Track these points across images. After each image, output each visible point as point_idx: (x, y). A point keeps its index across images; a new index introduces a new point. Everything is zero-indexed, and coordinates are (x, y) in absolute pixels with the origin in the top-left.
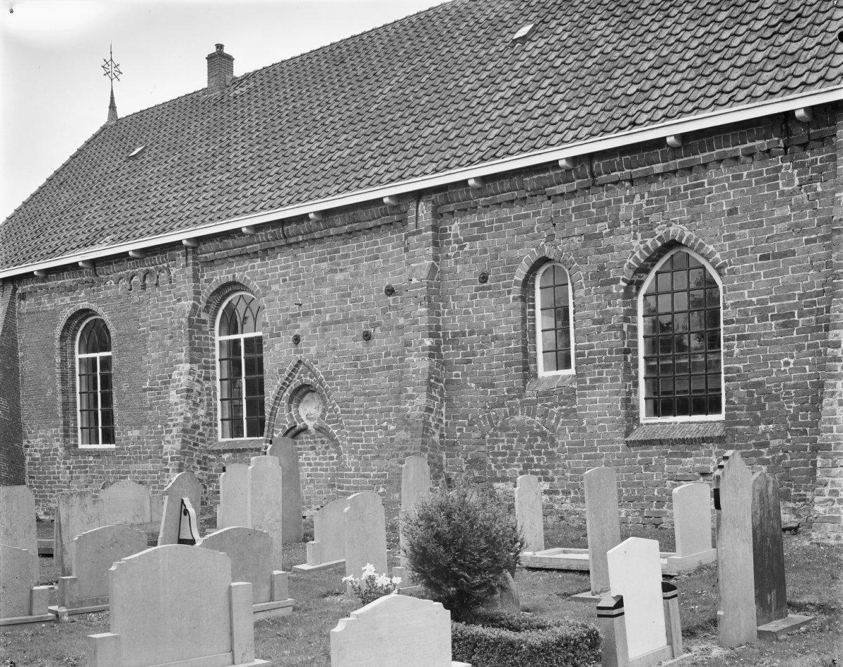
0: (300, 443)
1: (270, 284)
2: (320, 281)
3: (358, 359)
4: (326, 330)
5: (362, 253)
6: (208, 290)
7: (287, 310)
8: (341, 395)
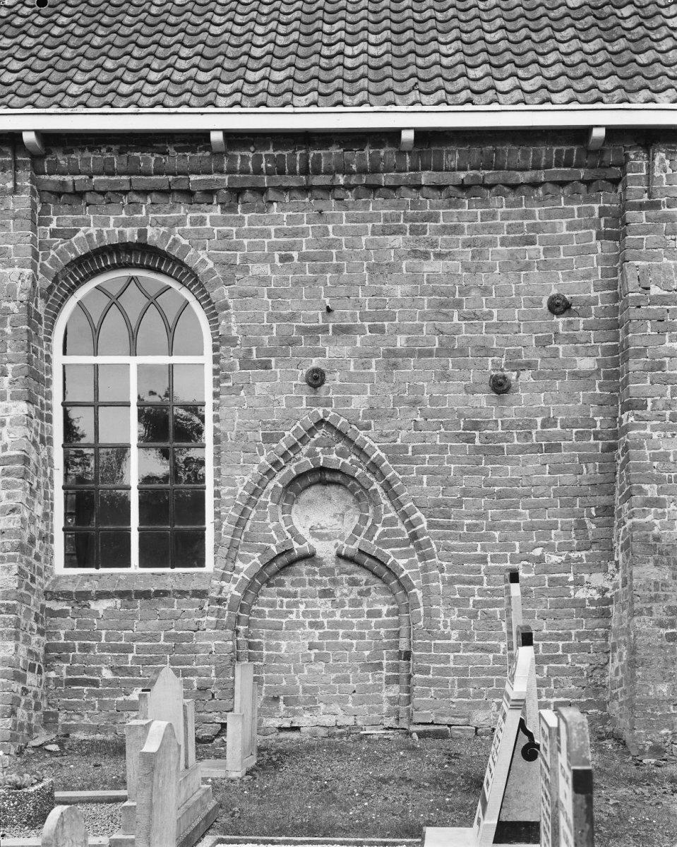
0: (293, 584)
1: (245, 259)
2: (381, 270)
3: (476, 426)
4: (395, 366)
5: (496, 229)
6: (61, 253)
7: (293, 317)
8: (428, 490)
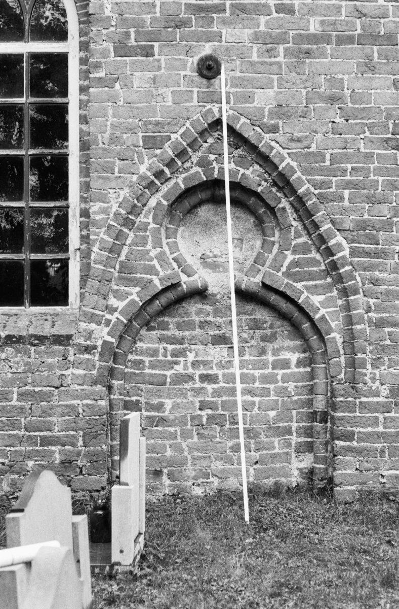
0: (179, 327)
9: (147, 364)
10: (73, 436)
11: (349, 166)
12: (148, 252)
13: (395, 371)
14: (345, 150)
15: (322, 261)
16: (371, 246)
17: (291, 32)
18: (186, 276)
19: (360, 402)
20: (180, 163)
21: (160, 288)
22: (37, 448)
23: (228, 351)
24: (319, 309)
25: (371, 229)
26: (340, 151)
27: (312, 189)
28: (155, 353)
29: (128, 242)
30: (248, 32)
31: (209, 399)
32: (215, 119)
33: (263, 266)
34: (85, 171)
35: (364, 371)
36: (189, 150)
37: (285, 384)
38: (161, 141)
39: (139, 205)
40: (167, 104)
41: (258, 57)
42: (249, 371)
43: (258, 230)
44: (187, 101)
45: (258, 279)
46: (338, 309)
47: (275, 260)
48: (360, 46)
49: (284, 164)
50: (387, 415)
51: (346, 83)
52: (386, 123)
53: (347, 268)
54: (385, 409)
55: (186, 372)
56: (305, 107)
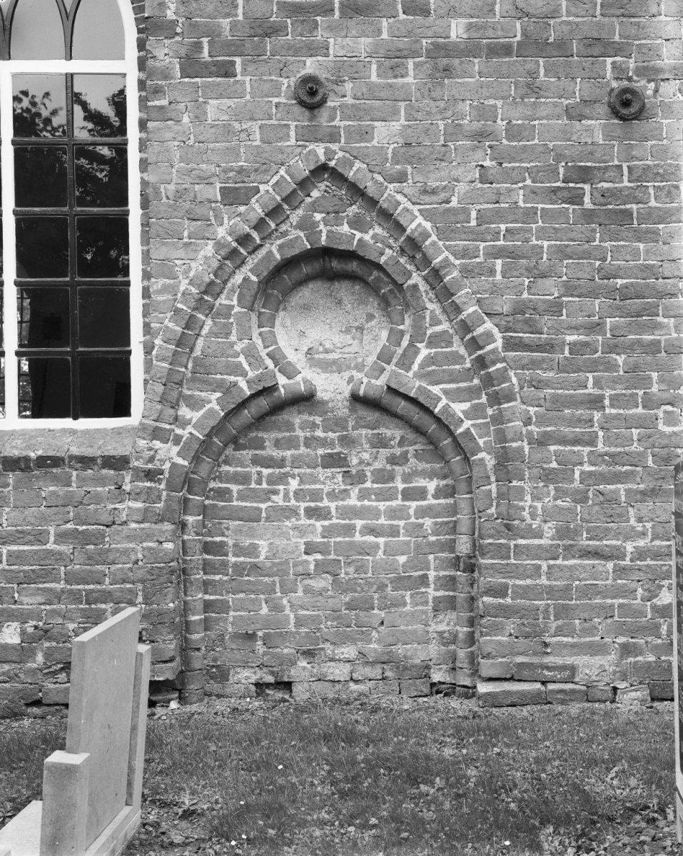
0: (277, 444)
3: (585, 175)
9: (235, 494)
10: (130, 590)
11: (503, 227)
12: (232, 345)
13: (565, 503)
14: (497, 205)
15: (466, 356)
16: (532, 336)
17: (424, 41)
18: (285, 378)
19: (516, 546)
20: (273, 225)
21: (249, 393)
22: (82, 606)
23: (343, 476)
24: (462, 421)
25: (532, 312)
26: (494, 206)
27: (452, 258)
28: (244, 479)
29: (204, 332)
30: (364, 43)
31: (318, 540)
32: (320, 163)
33: (389, 364)
34: (146, 239)
35: (521, 504)
36: (286, 207)
37: (420, 521)
38: (246, 194)
39: (218, 281)
40: (255, 143)
41: (378, 76)
42: (370, 503)
43: (384, 316)
44: (281, 139)
45: (381, 382)
46: (488, 420)
47: (404, 355)
48: (521, 58)
49: (413, 226)
50: (552, 562)
51: (500, 111)
52: (554, 167)
53: (499, 366)
54: (549, 555)
55: (287, 504)
56: (444, 146)
